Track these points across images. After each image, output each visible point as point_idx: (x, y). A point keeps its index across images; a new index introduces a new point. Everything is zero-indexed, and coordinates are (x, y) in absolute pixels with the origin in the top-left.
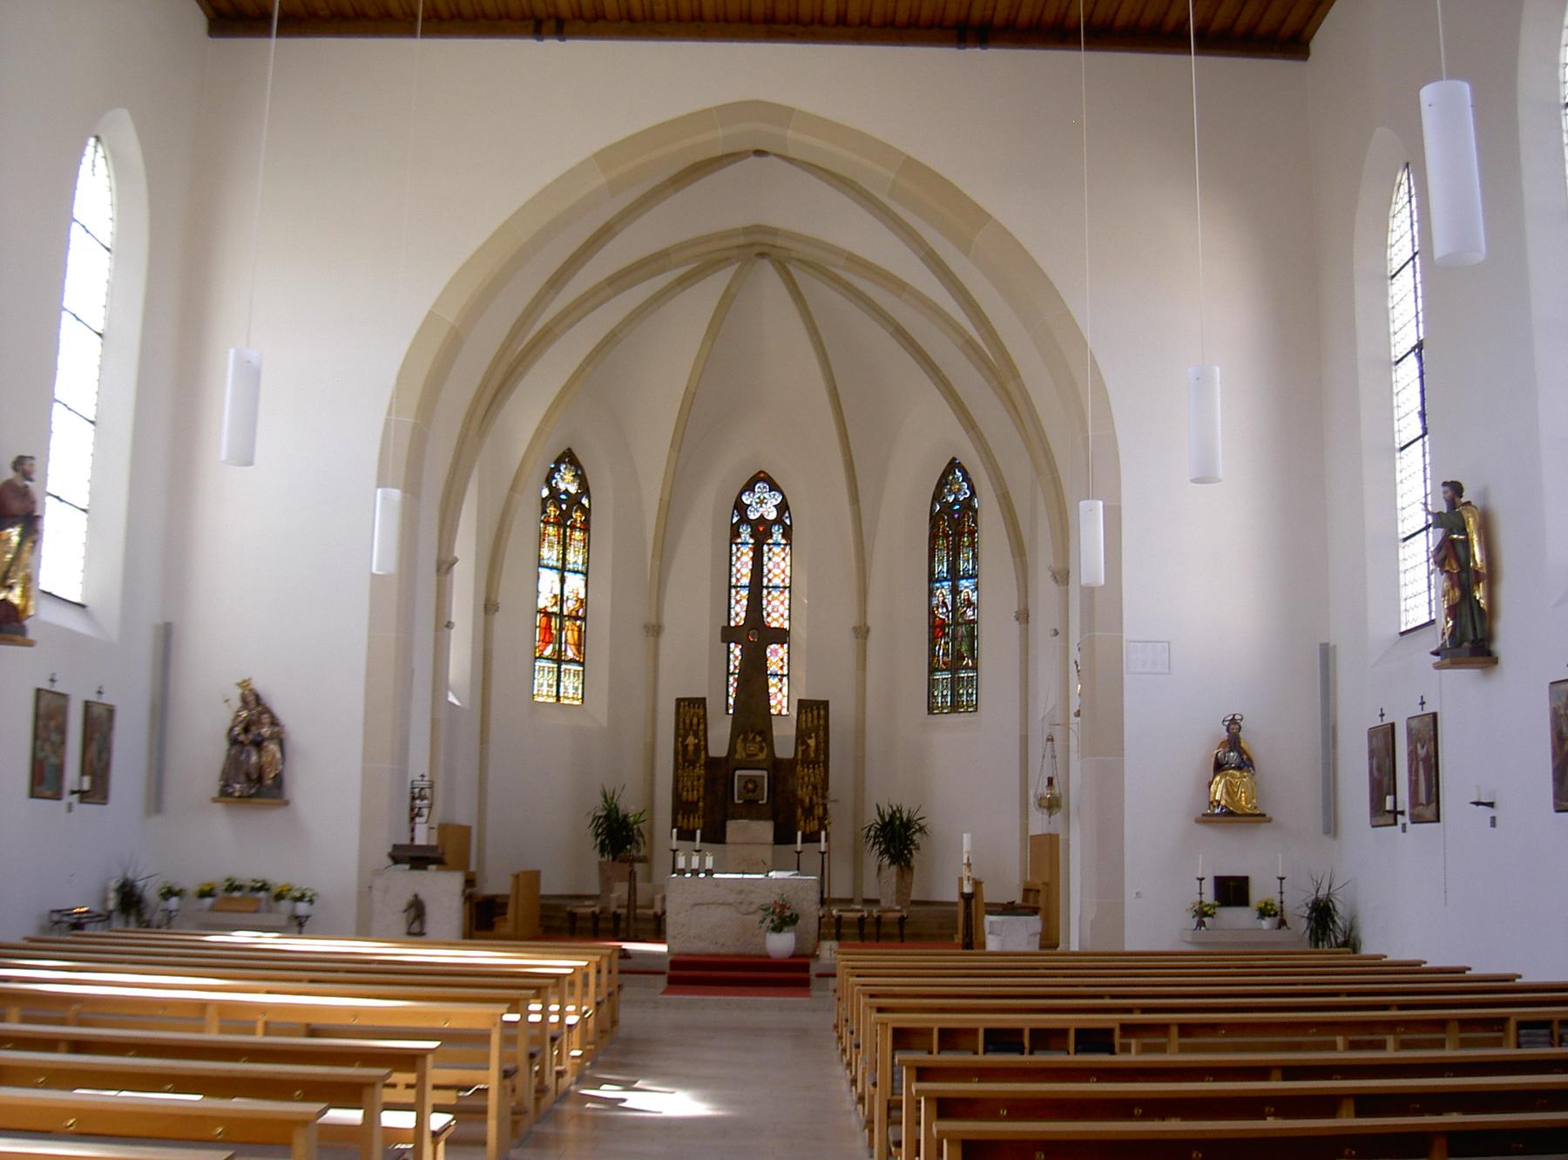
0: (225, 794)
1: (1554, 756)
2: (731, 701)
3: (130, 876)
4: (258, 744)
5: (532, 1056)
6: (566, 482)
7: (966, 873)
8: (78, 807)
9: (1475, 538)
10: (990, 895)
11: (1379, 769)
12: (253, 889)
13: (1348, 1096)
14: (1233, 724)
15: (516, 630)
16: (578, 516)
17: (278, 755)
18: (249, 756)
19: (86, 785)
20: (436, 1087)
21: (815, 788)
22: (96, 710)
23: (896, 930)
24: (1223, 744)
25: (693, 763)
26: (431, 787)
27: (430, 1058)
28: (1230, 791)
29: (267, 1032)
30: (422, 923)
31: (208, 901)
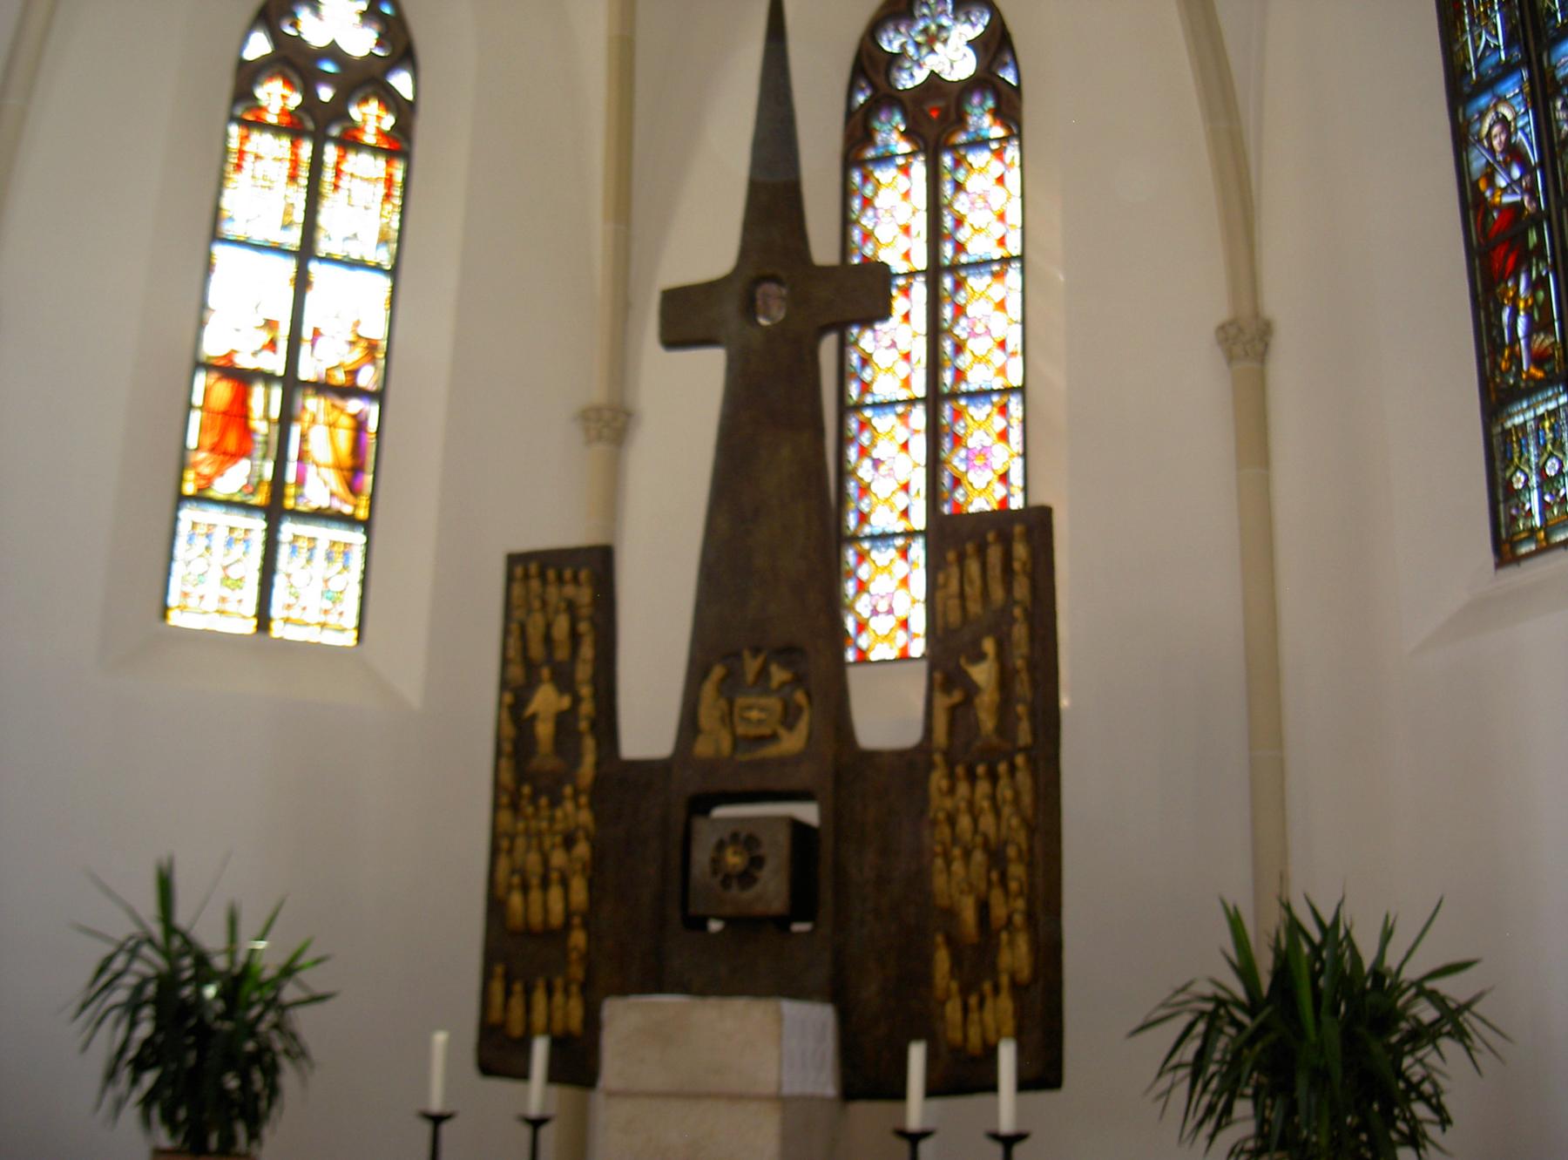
21: (996, 857)
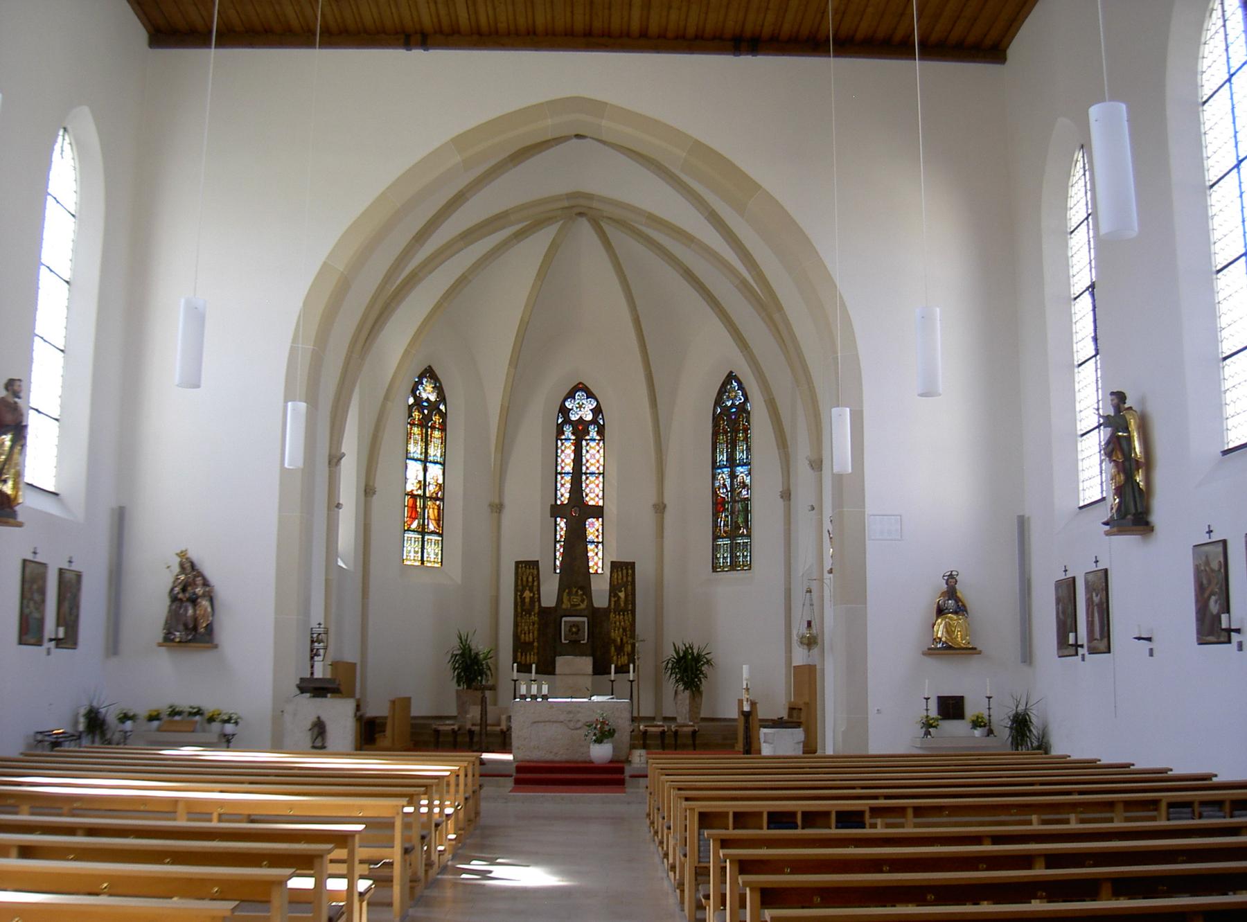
0: (168, 639)
1: (1197, 601)
2: (558, 563)
3: (95, 704)
4: (194, 601)
5: (423, 838)
6: (428, 392)
7: (745, 696)
8: (55, 651)
9: (1135, 435)
10: (762, 713)
11: (1064, 613)
12: (190, 714)
13: (1040, 855)
14: (951, 579)
15: (389, 509)
16: (436, 419)
17: (209, 609)
18: (186, 610)
19: (61, 635)
20: (362, 862)
21: (624, 630)
22: (68, 575)
23: (690, 742)
24: (943, 594)
25: (529, 612)
26: (326, 633)
27: (357, 837)
28: (949, 630)
29: (220, 820)
30: (323, 740)
31: (156, 723)
